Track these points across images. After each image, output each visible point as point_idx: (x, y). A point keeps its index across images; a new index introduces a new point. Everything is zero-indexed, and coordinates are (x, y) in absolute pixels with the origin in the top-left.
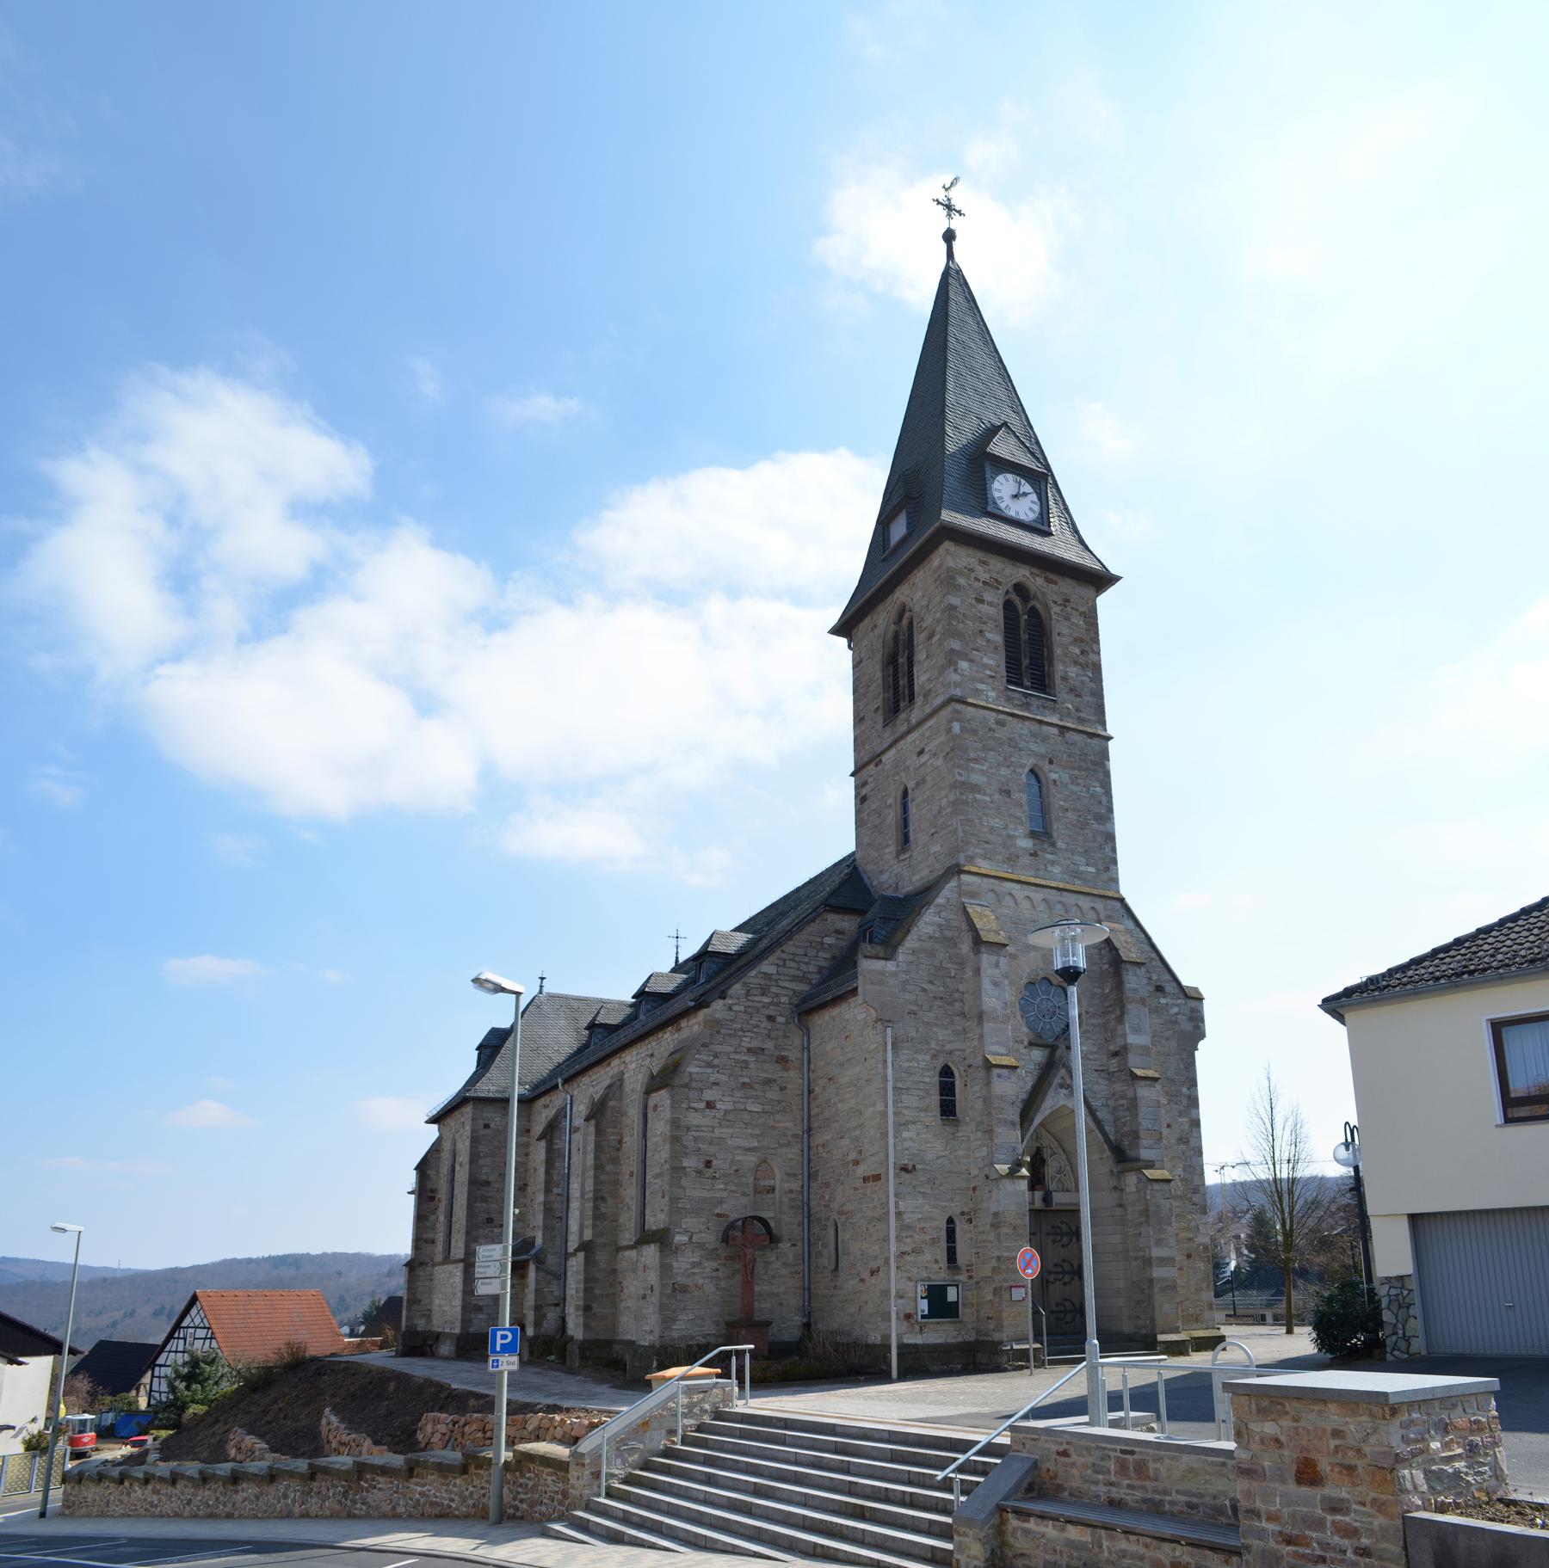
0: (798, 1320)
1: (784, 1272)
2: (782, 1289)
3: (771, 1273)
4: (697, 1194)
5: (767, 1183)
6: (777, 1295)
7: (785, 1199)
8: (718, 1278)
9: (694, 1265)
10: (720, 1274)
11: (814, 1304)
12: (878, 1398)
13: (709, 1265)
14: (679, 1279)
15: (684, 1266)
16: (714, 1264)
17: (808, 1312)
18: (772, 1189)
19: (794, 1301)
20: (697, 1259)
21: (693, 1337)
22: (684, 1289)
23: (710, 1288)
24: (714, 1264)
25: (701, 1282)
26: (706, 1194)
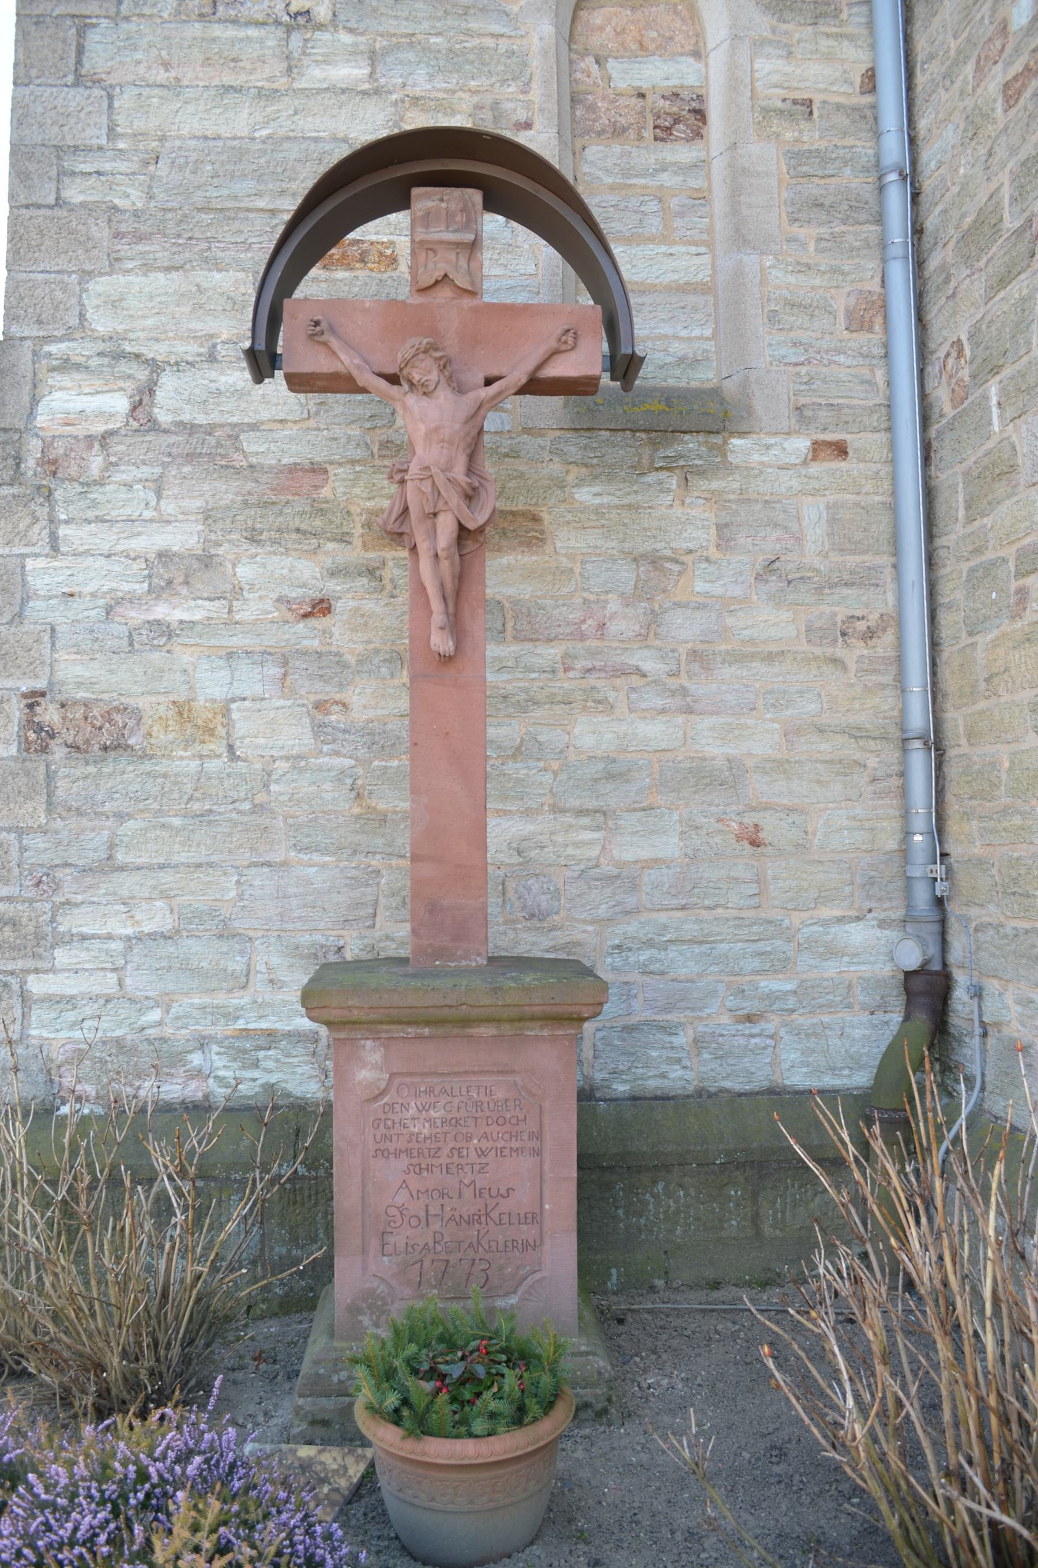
0: (876, 950)
1: (771, 622)
2: (762, 741)
3: (684, 628)
4: (191, 120)
5: (657, 73)
6: (726, 778)
7: (765, 155)
8: (330, 665)
9: (168, 573)
10: (339, 633)
11: (966, 841)
12: (441, 106)
13: (270, 575)
14: (75, 672)
15: (97, 578)
16: (305, 572)
17: (73, 173)
18: (684, 117)
19: (847, 821)
20: (183, 538)
21: (166, 1058)
22: (108, 735)
23: (273, 728)
24: (305, 572)
25: (212, 684)
26: (240, 121)
